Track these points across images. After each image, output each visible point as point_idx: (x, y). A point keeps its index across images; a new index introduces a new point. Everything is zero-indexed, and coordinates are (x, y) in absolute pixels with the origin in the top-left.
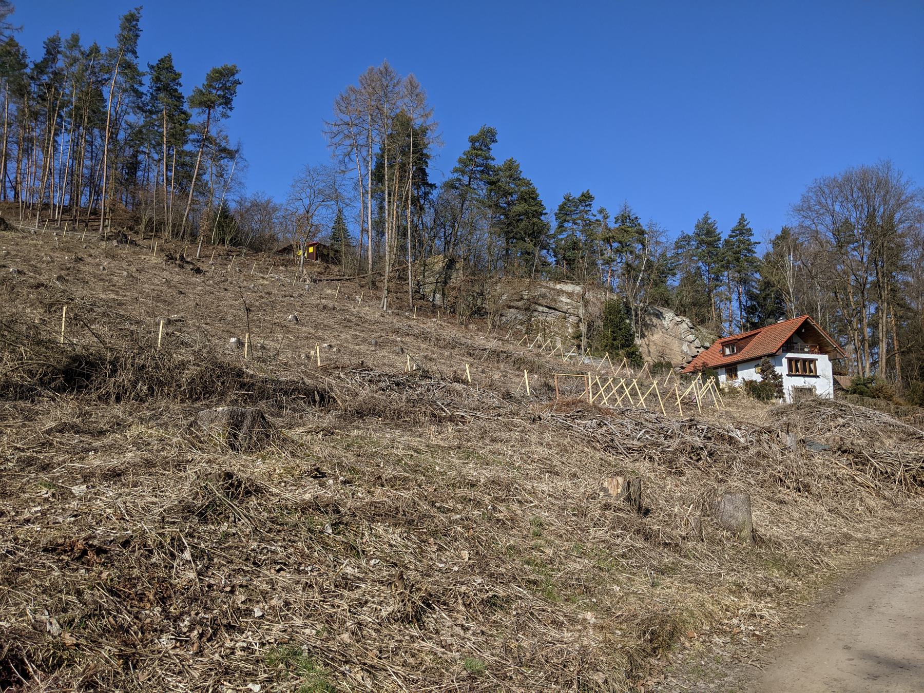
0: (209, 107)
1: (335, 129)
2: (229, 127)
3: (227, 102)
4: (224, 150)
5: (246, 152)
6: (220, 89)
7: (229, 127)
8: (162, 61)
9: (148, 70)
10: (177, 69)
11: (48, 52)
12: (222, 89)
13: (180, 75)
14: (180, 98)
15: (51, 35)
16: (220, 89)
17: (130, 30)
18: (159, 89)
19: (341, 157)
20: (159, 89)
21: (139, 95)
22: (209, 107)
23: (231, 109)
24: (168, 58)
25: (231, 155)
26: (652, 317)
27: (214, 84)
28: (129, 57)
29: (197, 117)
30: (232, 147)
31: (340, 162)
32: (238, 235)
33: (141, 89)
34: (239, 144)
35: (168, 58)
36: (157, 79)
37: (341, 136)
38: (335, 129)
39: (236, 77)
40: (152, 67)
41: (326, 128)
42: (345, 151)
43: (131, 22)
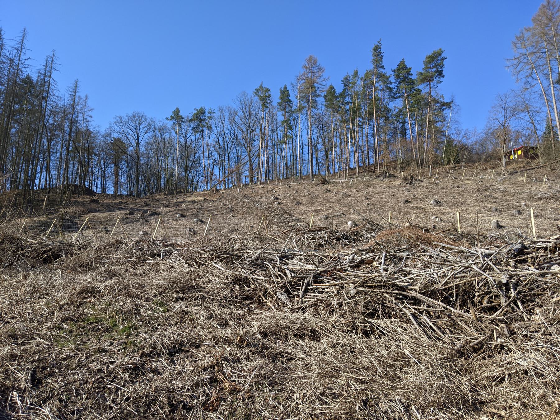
0: (429, 81)
1: (515, 62)
2: (443, 90)
3: (440, 73)
4: (444, 104)
5: (457, 101)
6: (434, 67)
7: (443, 90)
8: (399, 65)
9: (393, 73)
10: (408, 67)
11: (345, 85)
12: (435, 65)
13: (410, 69)
14: (413, 82)
15: (345, 75)
16: (434, 67)
17: (378, 55)
18: (400, 83)
19: (524, 80)
20: (400, 83)
21: (390, 89)
22: (429, 81)
23: (443, 77)
24: (403, 62)
25: (448, 105)
26: (113, 165)
27: (429, 66)
28: (381, 70)
29: (423, 88)
30: (447, 100)
31: (525, 83)
32: (459, 156)
33: (391, 86)
34: (453, 97)
35: (403, 62)
36: (398, 77)
37: (522, 64)
38: (515, 62)
39: (442, 56)
40: (394, 71)
41: (508, 63)
42: (527, 74)
43: (377, 51)
